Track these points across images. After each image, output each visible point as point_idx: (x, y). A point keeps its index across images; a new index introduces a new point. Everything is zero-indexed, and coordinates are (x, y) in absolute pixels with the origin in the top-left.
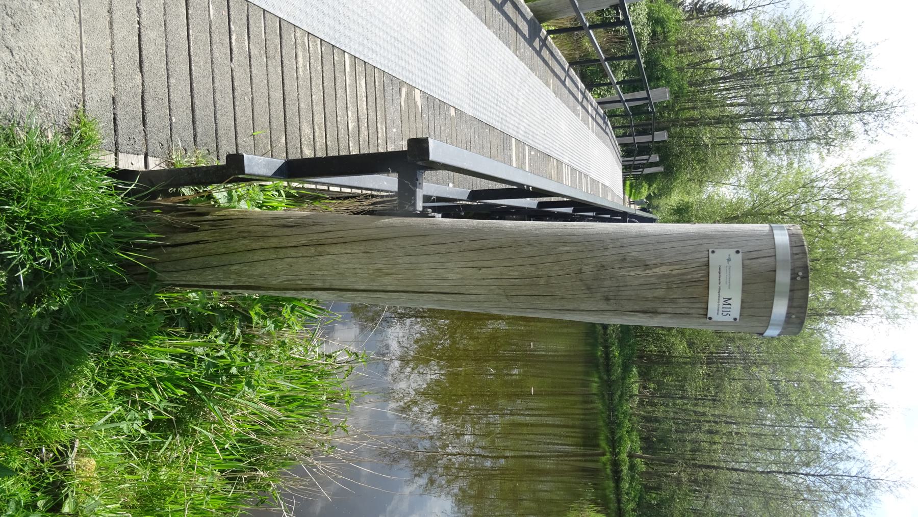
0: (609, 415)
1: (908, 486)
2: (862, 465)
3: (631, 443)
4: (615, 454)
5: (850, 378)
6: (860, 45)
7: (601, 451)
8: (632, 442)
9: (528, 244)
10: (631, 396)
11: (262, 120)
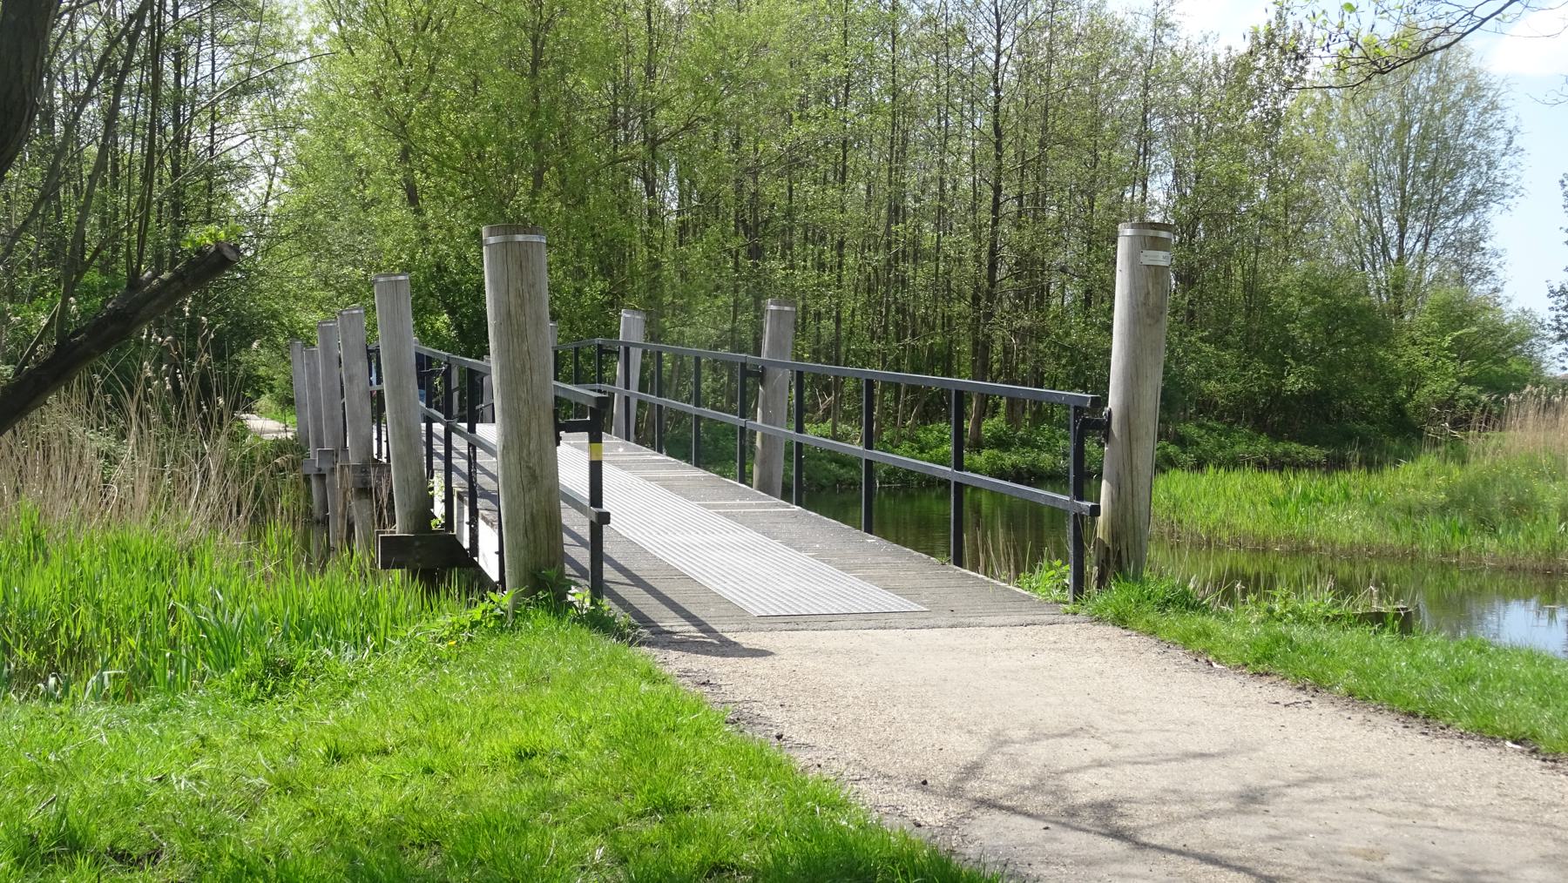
9: (1134, 352)
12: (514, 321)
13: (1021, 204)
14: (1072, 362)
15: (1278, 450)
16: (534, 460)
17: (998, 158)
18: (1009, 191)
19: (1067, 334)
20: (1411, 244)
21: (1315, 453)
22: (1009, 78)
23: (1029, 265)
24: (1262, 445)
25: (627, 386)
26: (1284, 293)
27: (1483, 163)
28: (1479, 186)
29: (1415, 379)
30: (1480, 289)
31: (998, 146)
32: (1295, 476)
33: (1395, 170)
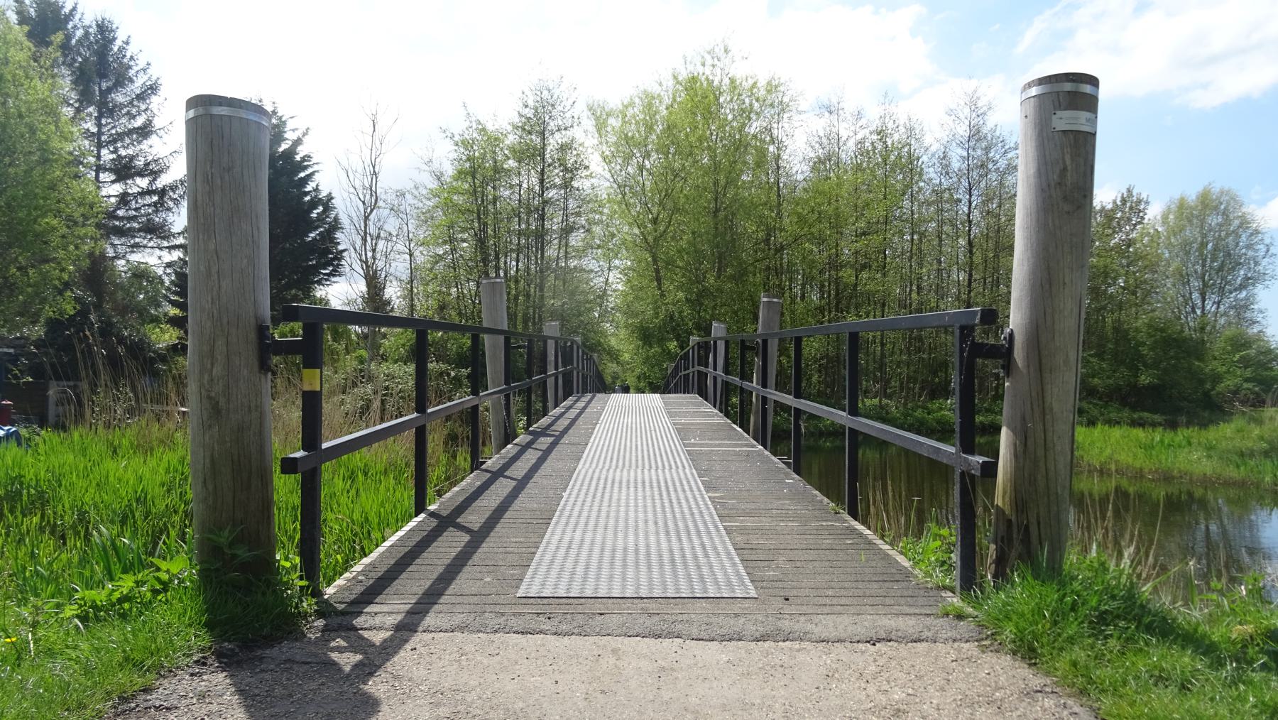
1: (975, 98)
2: (954, 144)
5: (847, 153)
6: (467, 132)
8: (941, 409)
10: (881, 407)
15: (1136, 416)
20: (1208, 307)
21: (1157, 418)
22: (976, 216)
24: (1126, 413)
25: (715, 369)
26: (1137, 330)
27: (1252, 262)
28: (1249, 275)
29: (1217, 378)
32: (1153, 431)
33: (1199, 268)
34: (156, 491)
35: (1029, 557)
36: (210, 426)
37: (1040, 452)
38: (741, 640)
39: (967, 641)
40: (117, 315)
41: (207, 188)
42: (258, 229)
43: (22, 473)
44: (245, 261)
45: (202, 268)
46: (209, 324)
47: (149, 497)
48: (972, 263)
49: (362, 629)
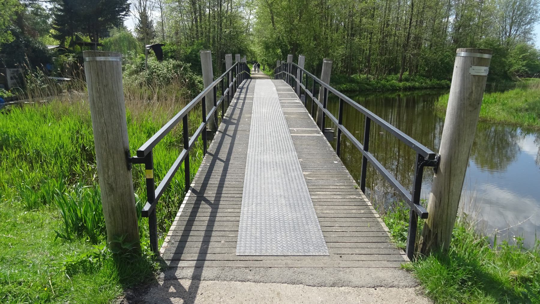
0: (379, 92)
3: (393, 80)
4: (400, 89)
7: (397, 98)
8: (393, 79)
10: (368, 79)
11: (358, 224)
12: (96, 106)
13: (417, 23)
14: (425, 61)
16: (112, 179)
17: (412, 12)
18: (414, 20)
19: (425, 55)
23: (417, 38)
26: (480, 45)
28: (533, 18)
29: (511, 65)
30: (530, 43)
31: (412, 9)
33: (511, 14)
34: (66, 140)
35: (436, 247)
36: (110, 195)
37: (446, 207)
38: (325, 286)
39: (411, 287)
40: (32, 37)
41: (98, 95)
42: (121, 109)
43: (8, 131)
44: (117, 125)
45: (100, 130)
46: (105, 154)
47: (65, 145)
48: (412, 14)
49: (179, 279)
